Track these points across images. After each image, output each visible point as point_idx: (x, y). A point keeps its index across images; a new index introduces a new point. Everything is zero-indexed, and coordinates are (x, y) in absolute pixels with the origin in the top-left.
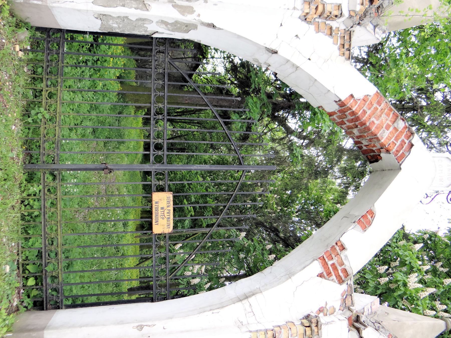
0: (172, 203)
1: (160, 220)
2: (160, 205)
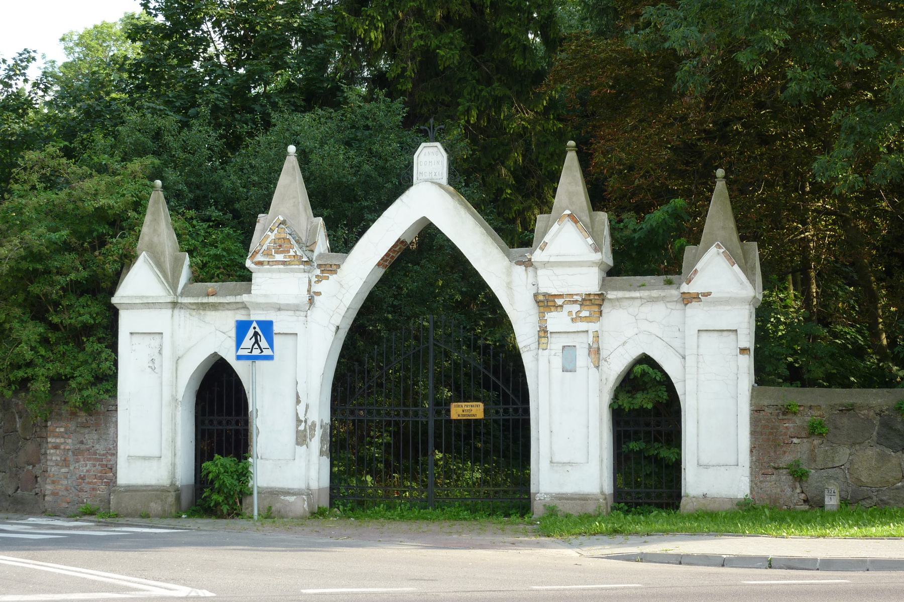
0: (459, 404)
1: (472, 413)
2: (461, 413)
